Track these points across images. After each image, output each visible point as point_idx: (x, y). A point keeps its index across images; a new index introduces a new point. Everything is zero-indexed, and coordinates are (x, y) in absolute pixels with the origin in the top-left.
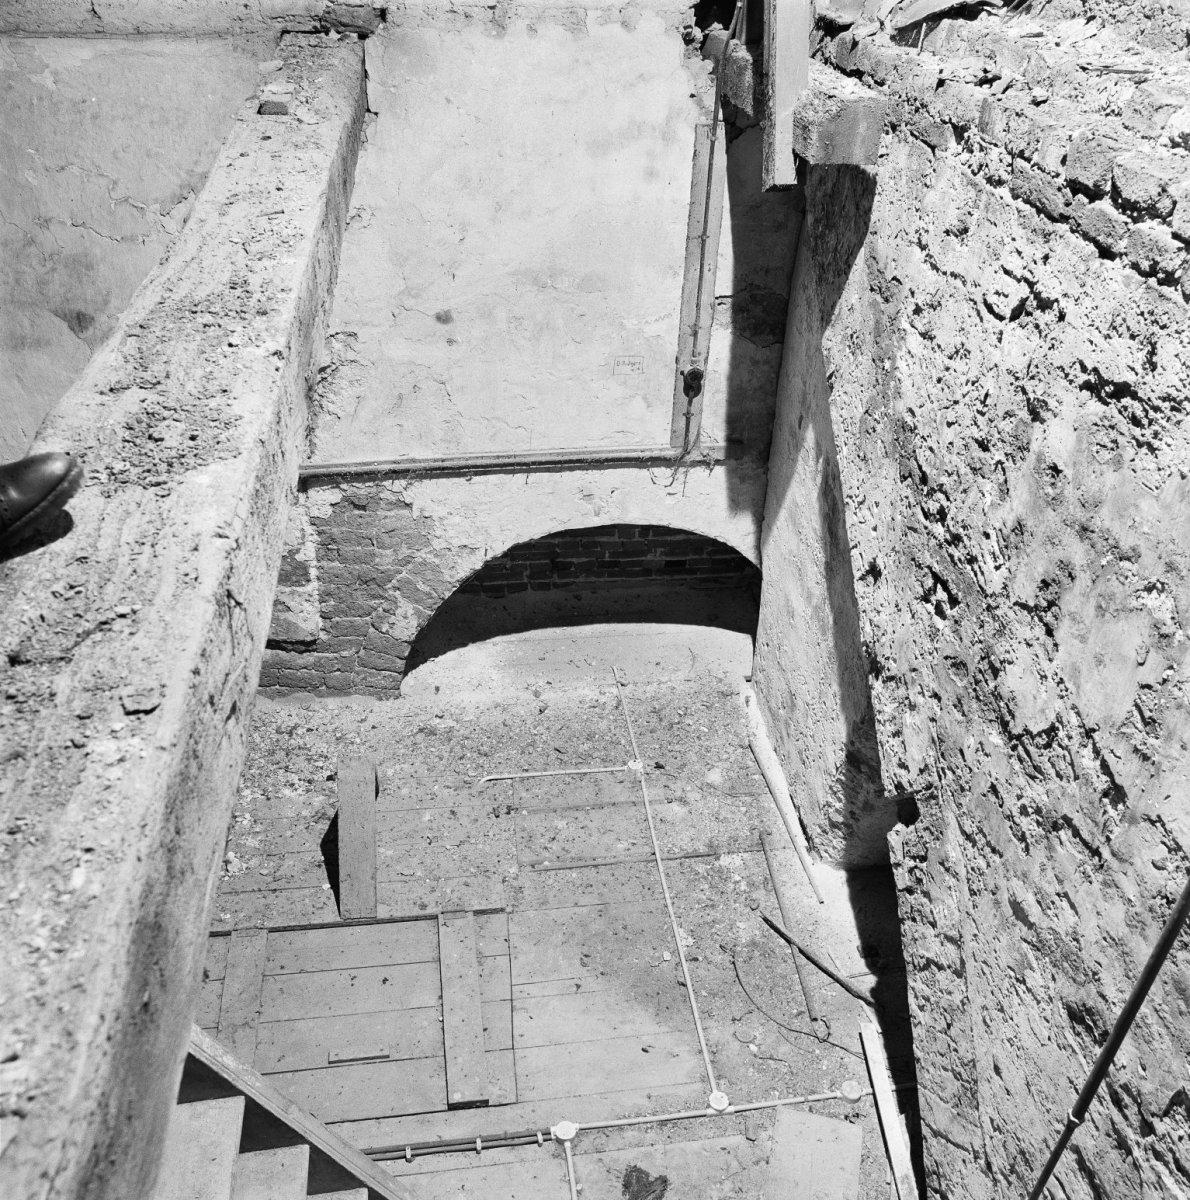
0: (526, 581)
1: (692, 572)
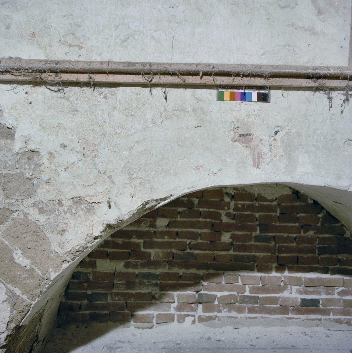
0: (172, 311)
1: (326, 312)
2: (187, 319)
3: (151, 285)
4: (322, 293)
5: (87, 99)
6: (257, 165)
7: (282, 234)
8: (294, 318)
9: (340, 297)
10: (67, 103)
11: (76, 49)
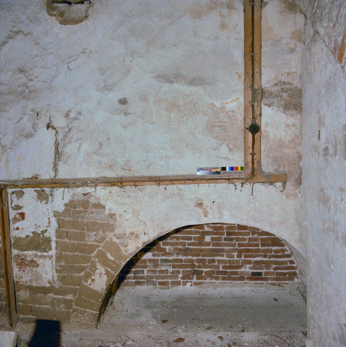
0: (179, 280)
2: (188, 283)
3: (167, 265)
4: (264, 269)
5: (134, 192)
6: (206, 216)
7: (239, 236)
8: (248, 283)
9: (274, 271)
10: (126, 194)
11: (128, 171)
